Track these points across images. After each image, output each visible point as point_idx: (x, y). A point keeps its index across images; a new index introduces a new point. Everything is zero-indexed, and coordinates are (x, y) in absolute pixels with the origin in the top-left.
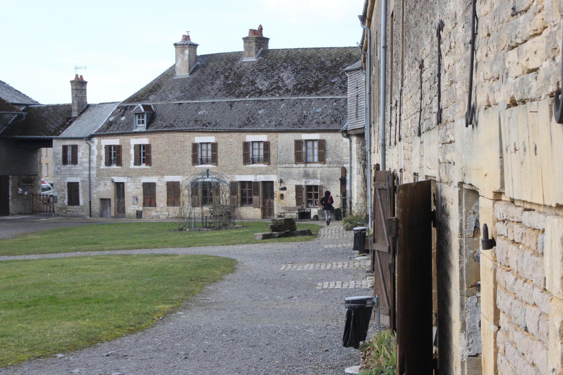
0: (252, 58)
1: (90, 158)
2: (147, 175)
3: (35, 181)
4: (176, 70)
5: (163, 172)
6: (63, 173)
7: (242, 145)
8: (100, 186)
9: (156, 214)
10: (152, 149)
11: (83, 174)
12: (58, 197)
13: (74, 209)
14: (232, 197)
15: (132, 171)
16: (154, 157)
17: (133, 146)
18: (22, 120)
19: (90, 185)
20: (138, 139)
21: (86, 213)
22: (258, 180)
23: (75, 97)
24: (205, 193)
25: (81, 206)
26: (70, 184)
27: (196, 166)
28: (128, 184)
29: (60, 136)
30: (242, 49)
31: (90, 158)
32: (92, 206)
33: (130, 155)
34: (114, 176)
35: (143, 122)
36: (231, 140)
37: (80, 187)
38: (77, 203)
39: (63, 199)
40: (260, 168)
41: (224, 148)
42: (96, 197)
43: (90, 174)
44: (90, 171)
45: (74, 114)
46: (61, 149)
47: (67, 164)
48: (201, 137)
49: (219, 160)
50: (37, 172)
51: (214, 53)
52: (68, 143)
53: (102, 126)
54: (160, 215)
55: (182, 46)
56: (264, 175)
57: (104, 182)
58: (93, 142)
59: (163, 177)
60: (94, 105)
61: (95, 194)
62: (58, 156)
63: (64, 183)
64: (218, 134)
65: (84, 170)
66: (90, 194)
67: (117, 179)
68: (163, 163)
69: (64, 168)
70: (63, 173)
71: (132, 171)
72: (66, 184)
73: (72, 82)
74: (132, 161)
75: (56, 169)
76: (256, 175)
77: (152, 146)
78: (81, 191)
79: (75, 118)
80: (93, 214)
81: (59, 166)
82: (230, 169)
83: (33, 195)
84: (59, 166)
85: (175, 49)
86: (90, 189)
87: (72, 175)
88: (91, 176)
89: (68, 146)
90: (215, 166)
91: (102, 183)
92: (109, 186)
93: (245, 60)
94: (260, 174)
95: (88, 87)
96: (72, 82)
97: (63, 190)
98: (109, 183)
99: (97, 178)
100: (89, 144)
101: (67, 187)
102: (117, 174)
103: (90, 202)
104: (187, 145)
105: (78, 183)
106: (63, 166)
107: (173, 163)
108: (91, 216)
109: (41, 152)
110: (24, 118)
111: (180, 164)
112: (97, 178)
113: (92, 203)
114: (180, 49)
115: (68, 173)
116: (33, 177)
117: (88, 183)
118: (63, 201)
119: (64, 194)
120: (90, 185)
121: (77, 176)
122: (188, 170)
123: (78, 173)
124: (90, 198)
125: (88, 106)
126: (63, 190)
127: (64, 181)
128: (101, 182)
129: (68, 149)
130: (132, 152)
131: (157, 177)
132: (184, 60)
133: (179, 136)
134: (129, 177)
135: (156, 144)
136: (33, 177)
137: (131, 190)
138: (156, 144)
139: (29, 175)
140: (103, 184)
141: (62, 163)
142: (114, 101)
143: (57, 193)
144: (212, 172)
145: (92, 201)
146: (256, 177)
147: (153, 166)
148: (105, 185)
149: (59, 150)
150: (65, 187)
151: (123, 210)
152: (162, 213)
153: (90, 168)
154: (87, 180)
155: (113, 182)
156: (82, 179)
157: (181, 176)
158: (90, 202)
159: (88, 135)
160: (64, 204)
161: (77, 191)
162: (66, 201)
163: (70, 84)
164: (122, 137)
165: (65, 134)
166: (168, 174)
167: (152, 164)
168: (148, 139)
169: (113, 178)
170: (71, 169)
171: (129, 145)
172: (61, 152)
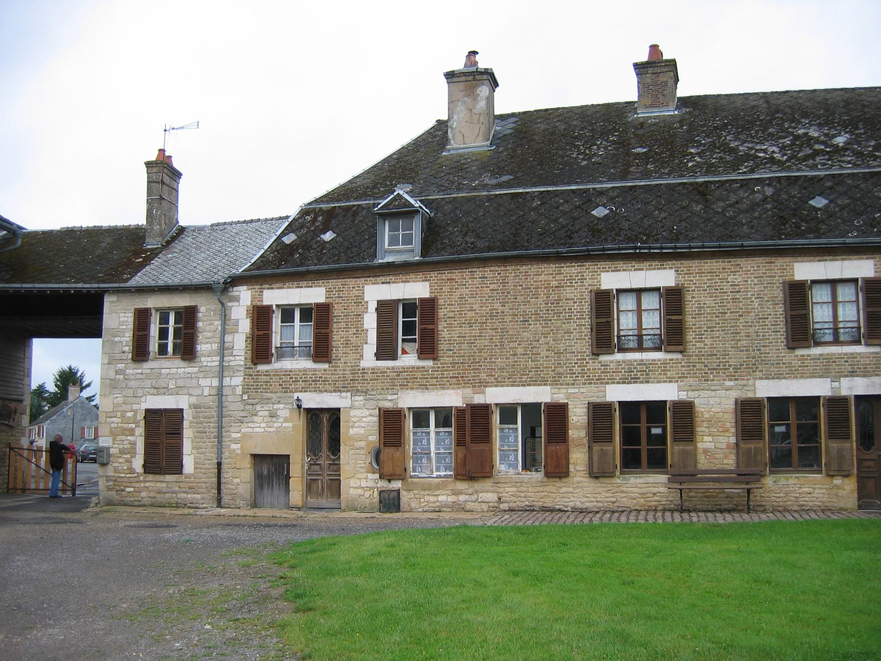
0: (665, 109)
1: (223, 342)
2: (424, 387)
3: (18, 414)
4: (450, 135)
5: (483, 376)
6: (132, 383)
7: (779, 294)
8: (255, 419)
9: (451, 499)
10: (441, 313)
11: (199, 386)
12: (112, 451)
13: (164, 485)
14: (742, 445)
15: (369, 376)
16: (445, 332)
17: (372, 306)
18: (12, 247)
19: (221, 416)
20: (393, 285)
21: (203, 497)
22: (844, 393)
23: (152, 203)
24: (630, 436)
25: (188, 476)
26: (152, 416)
27: (604, 358)
28: (353, 413)
29: (129, 284)
30: (632, 95)
31: (223, 342)
32: (223, 475)
33: (361, 332)
34: (304, 390)
35: (408, 240)
36: (738, 279)
37: (186, 424)
38: (178, 468)
39: (128, 456)
40: (853, 356)
41: (709, 302)
42: (239, 452)
43: (221, 388)
44: (221, 378)
45: (151, 243)
46: (131, 320)
47: (147, 361)
48: (641, 274)
49: (690, 336)
50: (22, 395)
51: (532, 108)
52: (152, 302)
53: (262, 256)
54: (465, 501)
55: (471, 78)
56: (864, 376)
57: (270, 407)
58: (237, 299)
59: (483, 393)
60: (200, 229)
61: (236, 441)
62: (117, 339)
63: (135, 412)
64: (687, 263)
65: (201, 375)
66: (220, 442)
67: (312, 400)
68: (480, 350)
69: (134, 370)
70: (132, 383)
71: (369, 376)
72: (141, 416)
73: (148, 164)
74: (370, 348)
75: (112, 374)
76: (836, 378)
77: (441, 302)
78: (188, 433)
79: (155, 253)
80: (226, 499)
81: (121, 366)
82: (733, 362)
83: (11, 448)
84: (121, 366)
85: (447, 85)
86: (220, 428)
87: (160, 390)
88: (226, 391)
89: (153, 311)
90: (679, 356)
91: (263, 412)
92: (286, 420)
93: (642, 114)
94: (852, 374)
95: (184, 187)
96: (148, 164)
97: (132, 432)
98: (284, 411)
99: (245, 397)
100: (222, 304)
101: (142, 423)
102: (313, 383)
103: (219, 464)
104: (569, 296)
105: (182, 410)
106: (134, 365)
107: (520, 351)
108: (219, 504)
109: (30, 347)
110: (20, 242)
111: (544, 353)
112: (245, 397)
113: (224, 467)
114: (462, 86)
115: (148, 383)
116: (13, 405)
117: (214, 413)
118: (129, 461)
119: (133, 444)
120: (221, 416)
121: (178, 391)
122: (576, 369)
123: (180, 383)
124: (220, 453)
125: (182, 230)
126: (132, 432)
127: (135, 407)
128: (258, 407)
129: (153, 319)
130: (370, 321)
131: (460, 391)
132: (475, 111)
133: (571, 270)
134: (356, 392)
135: (456, 296)
136: (13, 405)
137: (362, 431)
138: (456, 296)
139: (7, 399)
140: (267, 413)
141: (130, 356)
142: (255, 217)
143: (110, 439)
144: (80, 471)
145: (224, 461)
146: (836, 384)
147: (445, 359)
148: (273, 415)
149: (121, 323)
150: (137, 423)
151: (335, 487)
152: (474, 497)
153: (222, 368)
154: (212, 401)
155: (299, 407)
156: (193, 400)
157: (548, 388)
158: (219, 464)
159: (221, 276)
160: (131, 471)
161: (176, 432)
162: (138, 463)
163: (144, 169)
164: (333, 283)
165: (138, 280)
166: (498, 383)
167: (441, 353)
168: (427, 284)
169: (301, 395)
170: (161, 374)
171: (360, 301)
172: (131, 326)
